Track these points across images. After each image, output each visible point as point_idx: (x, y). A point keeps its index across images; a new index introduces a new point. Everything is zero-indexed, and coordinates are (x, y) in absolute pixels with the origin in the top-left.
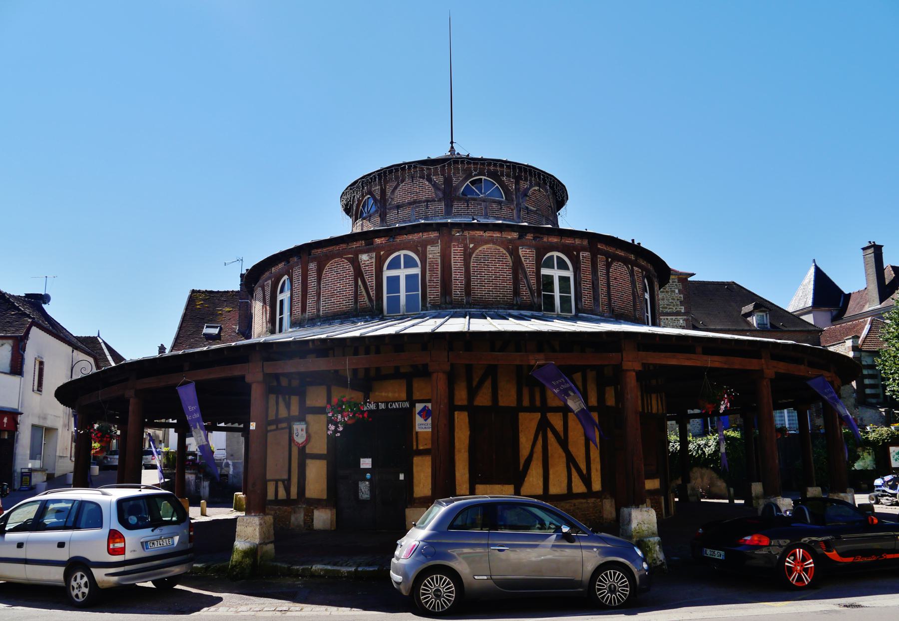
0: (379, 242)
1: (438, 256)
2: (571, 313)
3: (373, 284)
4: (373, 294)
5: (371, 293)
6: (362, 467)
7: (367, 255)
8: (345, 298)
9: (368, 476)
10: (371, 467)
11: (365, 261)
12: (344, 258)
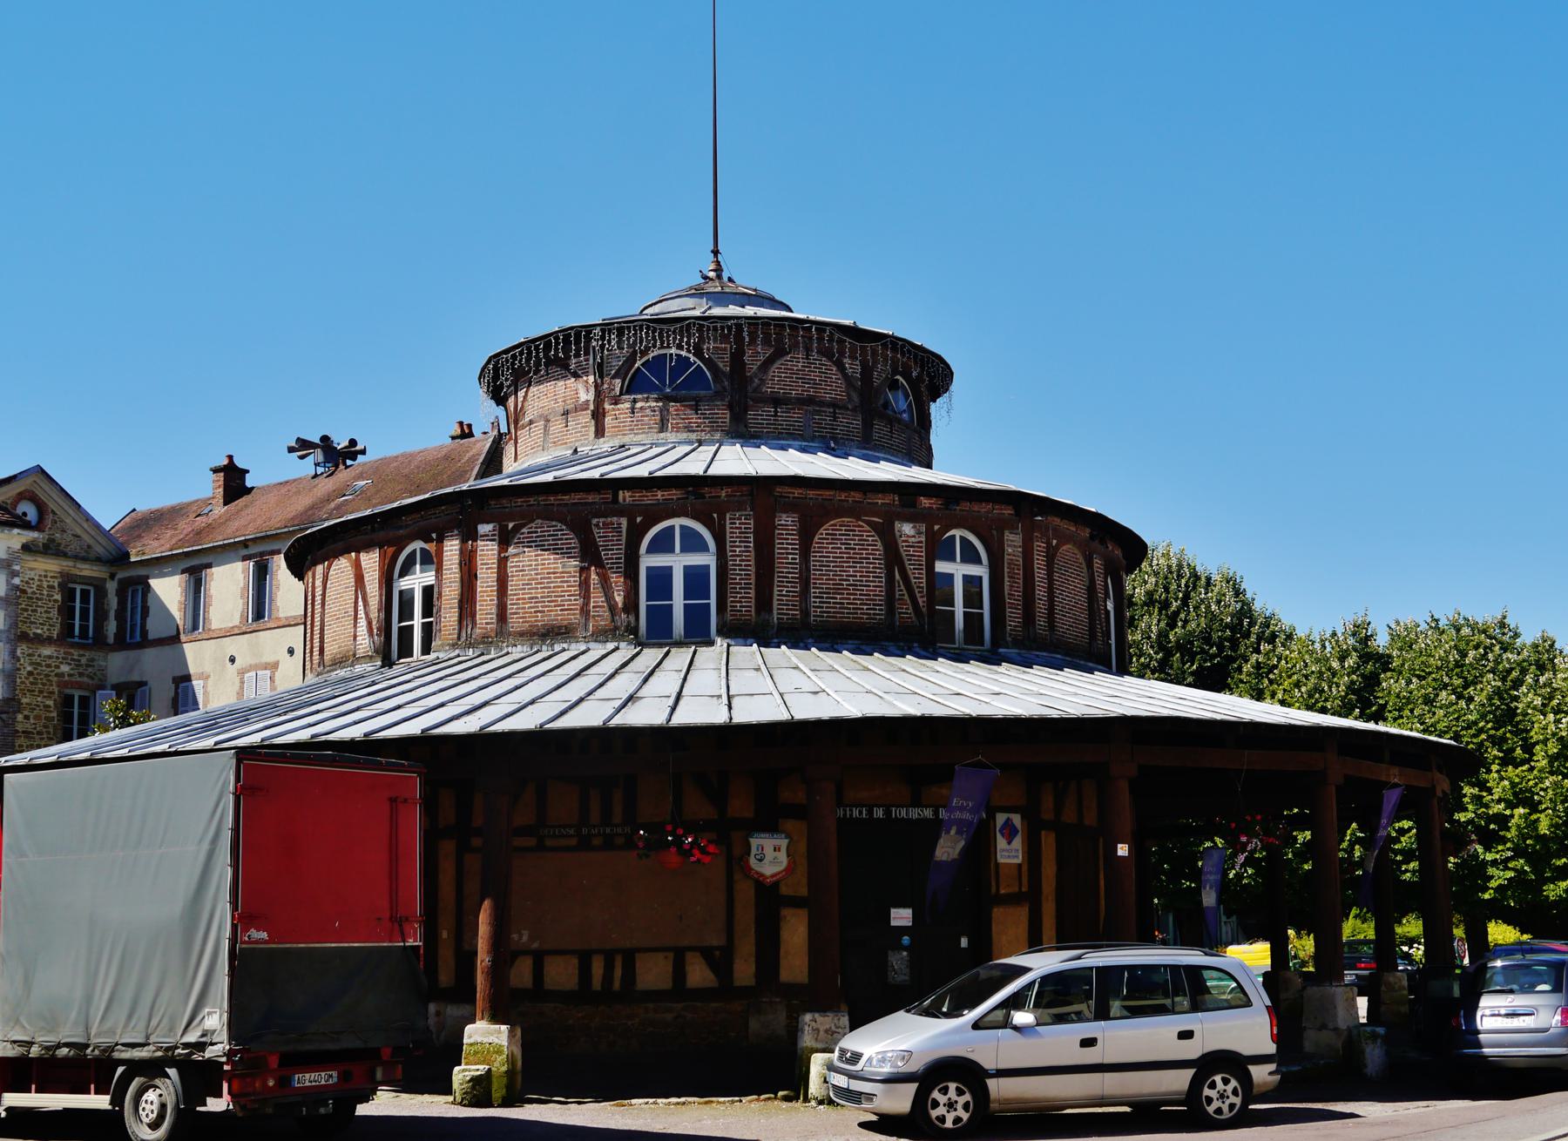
0: (927, 505)
1: (1019, 552)
2: (983, 645)
3: (922, 583)
4: (924, 602)
5: (920, 600)
6: (894, 923)
7: (911, 525)
8: (867, 600)
9: (906, 940)
10: (910, 924)
11: (908, 536)
12: (864, 521)
